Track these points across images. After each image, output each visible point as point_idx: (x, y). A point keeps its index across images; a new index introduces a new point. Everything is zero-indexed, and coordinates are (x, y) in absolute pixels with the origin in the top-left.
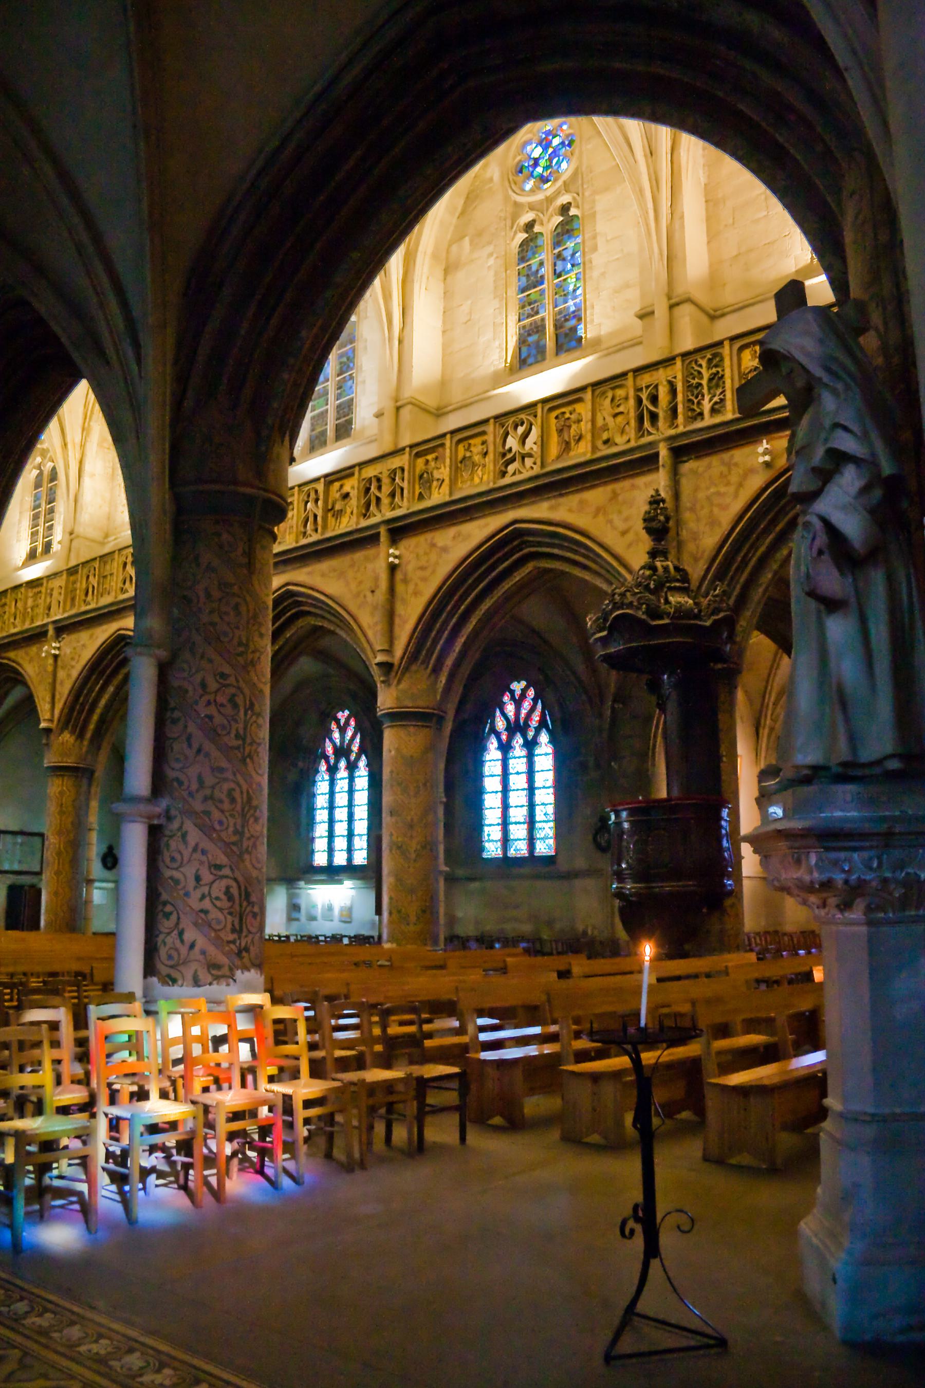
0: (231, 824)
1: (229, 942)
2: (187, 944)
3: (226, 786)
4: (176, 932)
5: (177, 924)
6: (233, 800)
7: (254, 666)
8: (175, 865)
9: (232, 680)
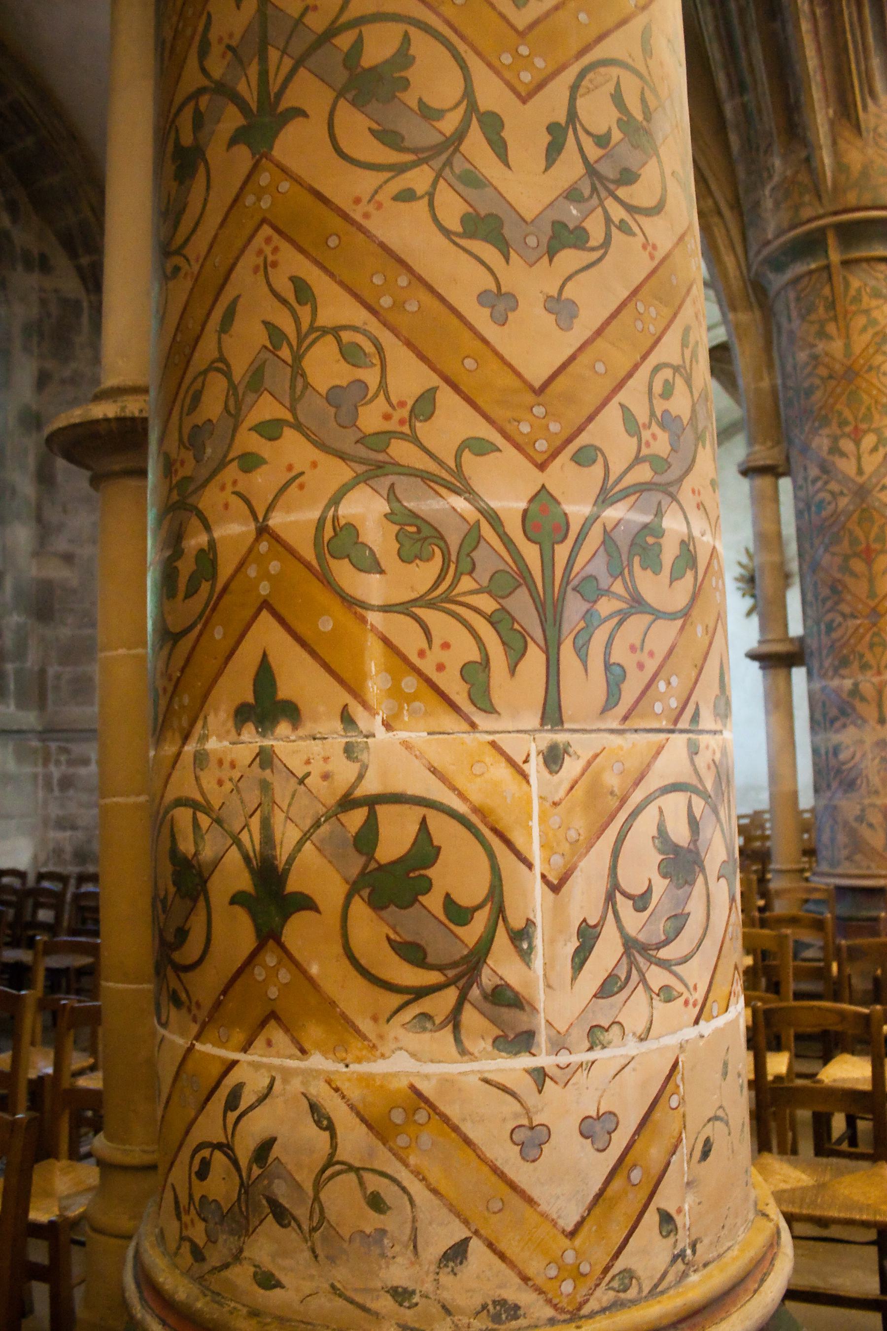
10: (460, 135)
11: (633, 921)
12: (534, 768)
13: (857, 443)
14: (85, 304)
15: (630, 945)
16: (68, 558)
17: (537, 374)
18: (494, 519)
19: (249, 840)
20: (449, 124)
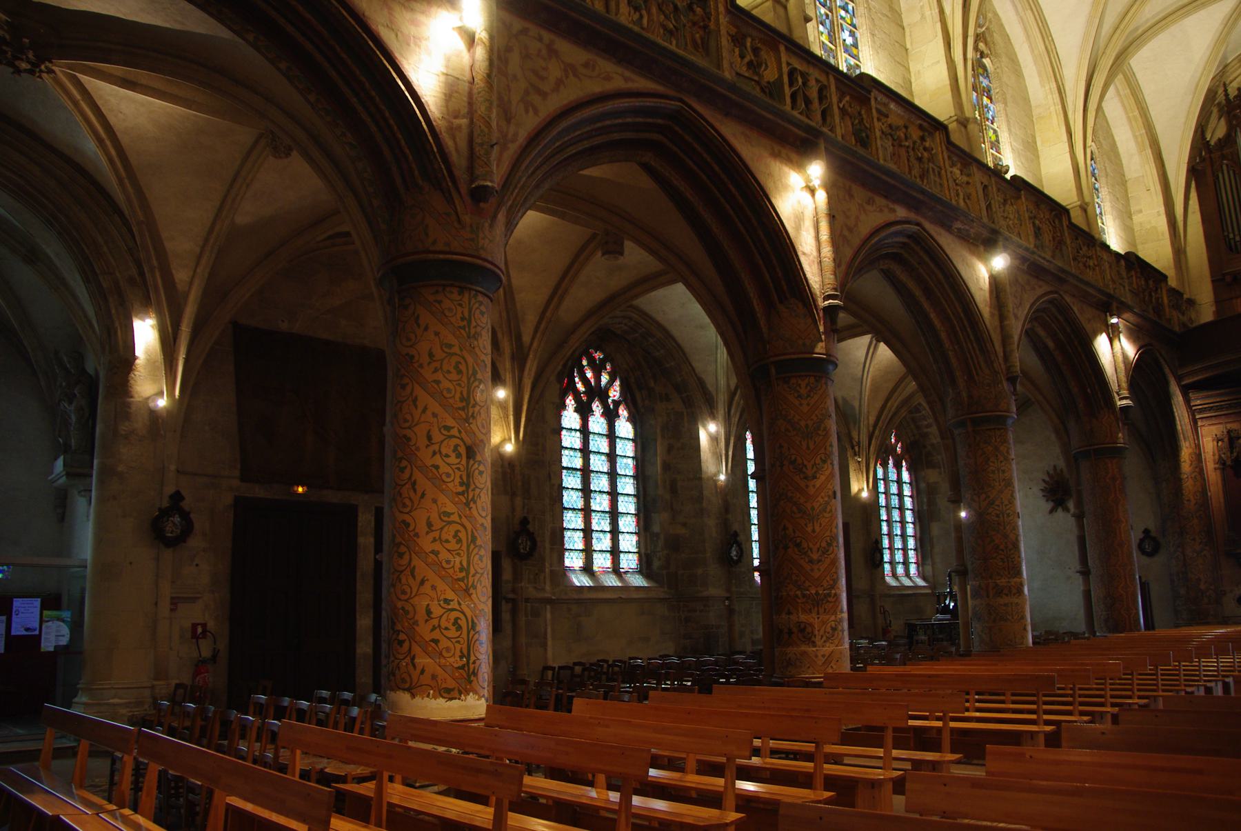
0: (458, 476)
1: (458, 494)
2: (419, 494)
3: (454, 360)
4: (408, 658)
5: (411, 393)
6: (459, 541)
7: (475, 502)
8: (407, 425)
9: (454, 432)
10: (807, 551)
11: (828, 635)
12: (816, 619)
13: (979, 497)
14: (685, 413)
15: (827, 637)
16: (684, 525)
17: (816, 577)
18: (811, 593)
19: (1191, 202)
20: (806, 550)
